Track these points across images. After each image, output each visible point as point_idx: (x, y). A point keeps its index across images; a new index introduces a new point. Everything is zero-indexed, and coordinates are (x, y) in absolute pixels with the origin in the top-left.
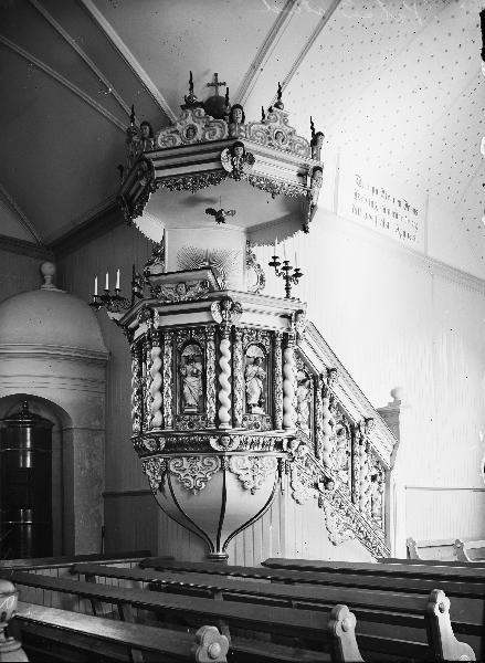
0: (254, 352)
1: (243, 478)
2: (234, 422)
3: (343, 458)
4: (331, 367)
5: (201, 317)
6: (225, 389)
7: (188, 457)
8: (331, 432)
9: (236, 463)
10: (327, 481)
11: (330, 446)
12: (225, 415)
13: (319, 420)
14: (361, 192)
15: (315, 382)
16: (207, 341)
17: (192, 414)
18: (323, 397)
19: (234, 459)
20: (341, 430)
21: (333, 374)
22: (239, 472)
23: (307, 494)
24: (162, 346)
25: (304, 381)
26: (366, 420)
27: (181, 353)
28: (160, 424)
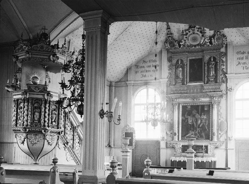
0: (54, 107)
1: (49, 141)
4: (70, 111)
5: (41, 97)
8: (69, 129)
9: (48, 137)
10: (67, 143)
11: (68, 133)
12: (46, 124)
13: (66, 125)
17: (37, 123)
18: (67, 119)
22: (48, 140)
23: (61, 145)
26: (78, 126)
27: (34, 105)
28: (26, 124)
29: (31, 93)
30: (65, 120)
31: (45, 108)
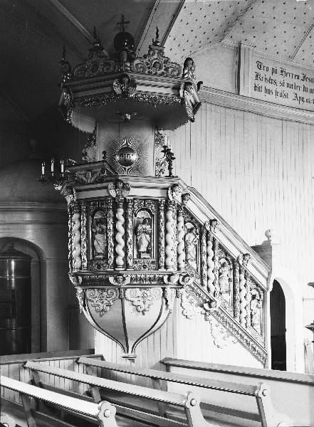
0: (142, 215)
1: (135, 303)
2: (127, 266)
3: (225, 284)
5: (102, 193)
6: (120, 244)
7: (98, 289)
12: (120, 261)
14: (262, 73)
15: (202, 231)
16: (108, 209)
17: (100, 259)
18: (207, 240)
19: (128, 291)
20: (224, 263)
21: (214, 223)
22: (132, 299)
23: (195, 311)
24: (80, 213)
25: (192, 229)
26: (244, 255)
27: (93, 216)
28: (79, 266)
29: (82, 188)
30: (201, 244)
31: (116, 220)
